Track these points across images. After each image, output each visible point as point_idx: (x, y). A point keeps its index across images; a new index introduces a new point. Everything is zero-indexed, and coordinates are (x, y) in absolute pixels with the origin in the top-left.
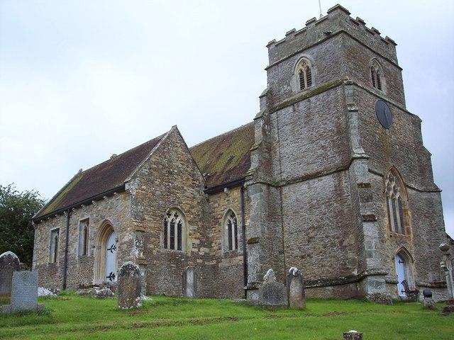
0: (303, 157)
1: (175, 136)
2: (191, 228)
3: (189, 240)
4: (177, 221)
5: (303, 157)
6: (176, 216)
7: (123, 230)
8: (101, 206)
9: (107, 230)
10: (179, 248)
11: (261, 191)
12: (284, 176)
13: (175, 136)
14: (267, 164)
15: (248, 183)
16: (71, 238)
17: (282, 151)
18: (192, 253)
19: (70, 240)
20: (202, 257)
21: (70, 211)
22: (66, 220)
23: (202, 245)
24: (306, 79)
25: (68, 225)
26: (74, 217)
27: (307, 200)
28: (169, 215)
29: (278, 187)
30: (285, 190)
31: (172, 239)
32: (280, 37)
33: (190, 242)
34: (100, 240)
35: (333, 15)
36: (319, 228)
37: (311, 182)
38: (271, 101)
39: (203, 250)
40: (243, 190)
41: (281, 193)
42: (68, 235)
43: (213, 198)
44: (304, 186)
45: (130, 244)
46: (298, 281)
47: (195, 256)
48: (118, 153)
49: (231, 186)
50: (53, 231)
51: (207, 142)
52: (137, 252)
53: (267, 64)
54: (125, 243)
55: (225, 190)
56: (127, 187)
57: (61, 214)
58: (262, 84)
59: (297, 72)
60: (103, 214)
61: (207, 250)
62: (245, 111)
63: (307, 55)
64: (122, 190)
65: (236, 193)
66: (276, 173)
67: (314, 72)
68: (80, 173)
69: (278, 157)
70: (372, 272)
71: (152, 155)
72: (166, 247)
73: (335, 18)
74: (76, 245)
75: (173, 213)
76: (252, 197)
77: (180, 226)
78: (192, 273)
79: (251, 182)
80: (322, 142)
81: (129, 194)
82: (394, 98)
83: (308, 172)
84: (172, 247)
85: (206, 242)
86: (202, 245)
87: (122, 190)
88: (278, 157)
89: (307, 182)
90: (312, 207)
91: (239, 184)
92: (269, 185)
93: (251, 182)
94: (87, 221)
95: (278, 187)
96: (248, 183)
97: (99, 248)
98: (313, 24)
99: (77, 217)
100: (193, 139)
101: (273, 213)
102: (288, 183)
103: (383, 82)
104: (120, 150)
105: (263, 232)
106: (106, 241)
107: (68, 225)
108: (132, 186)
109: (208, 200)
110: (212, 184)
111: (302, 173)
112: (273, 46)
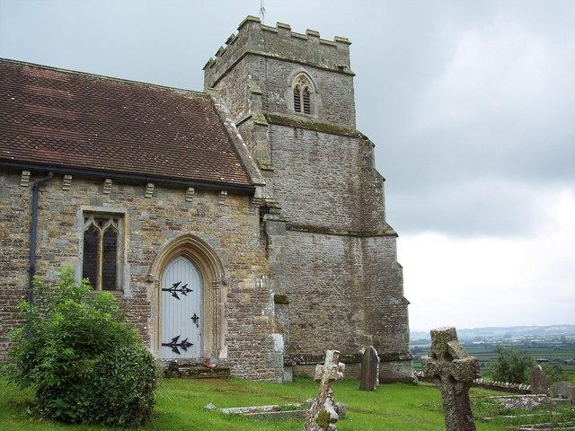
19: (43, 245)
27: (310, 257)
37: (317, 236)
44: (307, 239)
54: (246, 291)
79: (276, 218)
83: (312, 222)
93: (276, 218)
111: (302, 220)
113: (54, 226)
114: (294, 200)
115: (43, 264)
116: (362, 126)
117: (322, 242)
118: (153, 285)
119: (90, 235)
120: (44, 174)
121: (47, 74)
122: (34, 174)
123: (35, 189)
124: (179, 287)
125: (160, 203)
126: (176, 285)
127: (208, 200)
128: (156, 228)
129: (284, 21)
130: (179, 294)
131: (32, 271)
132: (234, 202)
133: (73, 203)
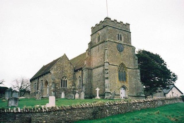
1: (65, 57)
2: (70, 81)
3: (69, 85)
4: (65, 80)
6: (65, 78)
7: (50, 83)
8: (45, 76)
9: (47, 83)
10: (66, 87)
11: (86, 71)
13: (65, 57)
14: (89, 63)
16: (39, 85)
18: (70, 88)
19: (39, 86)
20: (73, 89)
23: (73, 86)
24: (99, 39)
25: (38, 82)
26: (39, 79)
28: (63, 78)
29: (91, 70)
31: (64, 84)
32: (94, 26)
33: (69, 85)
35: (105, 20)
36: (100, 81)
38: (91, 45)
39: (73, 87)
40: (82, 71)
44: (97, 69)
45: (51, 86)
46: (78, 94)
47: (71, 89)
48: (45, 64)
49: (80, 69)
50: (41, 81)
51: (80, 56)
52: (53, 88)
53: (91, 34)
57: (37, 79)
58: (89, 40)
59: (97, 37)
61: (74, 87)
62: (83, 48)
63: (99, 32)
65: (81, 72)
67: (101, 37)
70: (107, 92)
71: (58, 63)
72: (62, 86)
73: (106, 21)
74: (40, 87)
75: (64, 78)
77: (66, 81)
78: (63, 93)
80: (101, 57)
81: (51, 73)
82: (126, 42)
84: (64, 87)
85: (74, 85)
86: (73, 86)
87: (49, 72)
91: (81, 69)
92: (89, 69)
94: (42, 80)
95: (91, 70)
97: (45, 87)
98: (101, 23)
99: (40, 79)
100: (70, 58)
101: (90, 76)
103: (123, 37)
104: (46, 64)
105: (86, 82)
106: (47, 86)
107: (38, 82)
108: (52, 72)
109: (75, 73)
110: (76, 69)
112: (92, 29)
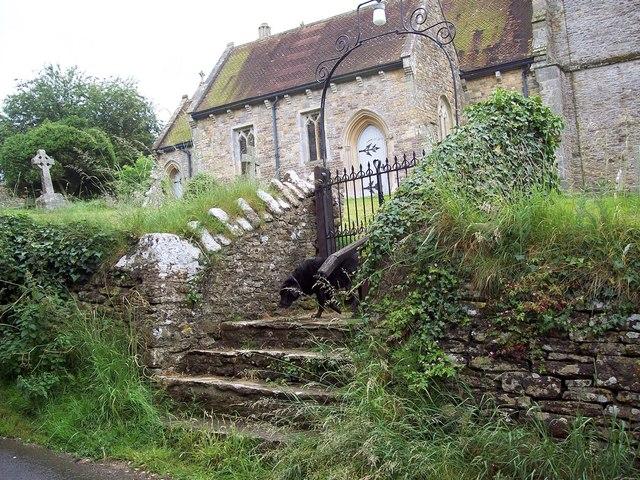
0: (606, 33)
5: (606, 33)
7: (403, 122)
12: (575, 58)
15: (538, 65)
17: (571, 25)
19: (282, 141)
21: (324, 86)
22: (271, 113)
27: (616, 89)
30: (580, 76)
34: (350, 138)
37: (622, 66)
41: (572, 79)
42: (276, 134)
43: (471, 86)
44: (611, 72)
48: (278, 28)
54: (407, 140)
55: (498, 74)
56: (406, 63)
60: (354, 102)
64: (396, 67)
66: (561, 54)
68: (232, 52)
69: (563, 33)
76: (543, 83)
79: (543, 64)
81: (409, 72)
83: (616, 54)
88: (563, 33)
89: (617, 65)
90: (624, 98)
93: (543, 64)
94: (247, 129)
96: (538, 65)
102: (585, 67)
106: (357, 140)
109: (464, 87)
111: (605, 54)
113: (286, 127)
114: (593, 37)
115: (283, 151)
116: (356, 8)
117: (629, 70)
118: (344, 150)
119: (310, 126)
120: (276, 98)
121: (314, 28)
122: (272, 100)
123: (275, 109)
124: (371, 147)
125: (343, 94)
126: (368, 147)
127: (374, 81)
128: (342, 111)
129: (5, 97)
130: (371, 152)
131: (277, 156)
132: (393, 76)
133: (294, 110)
